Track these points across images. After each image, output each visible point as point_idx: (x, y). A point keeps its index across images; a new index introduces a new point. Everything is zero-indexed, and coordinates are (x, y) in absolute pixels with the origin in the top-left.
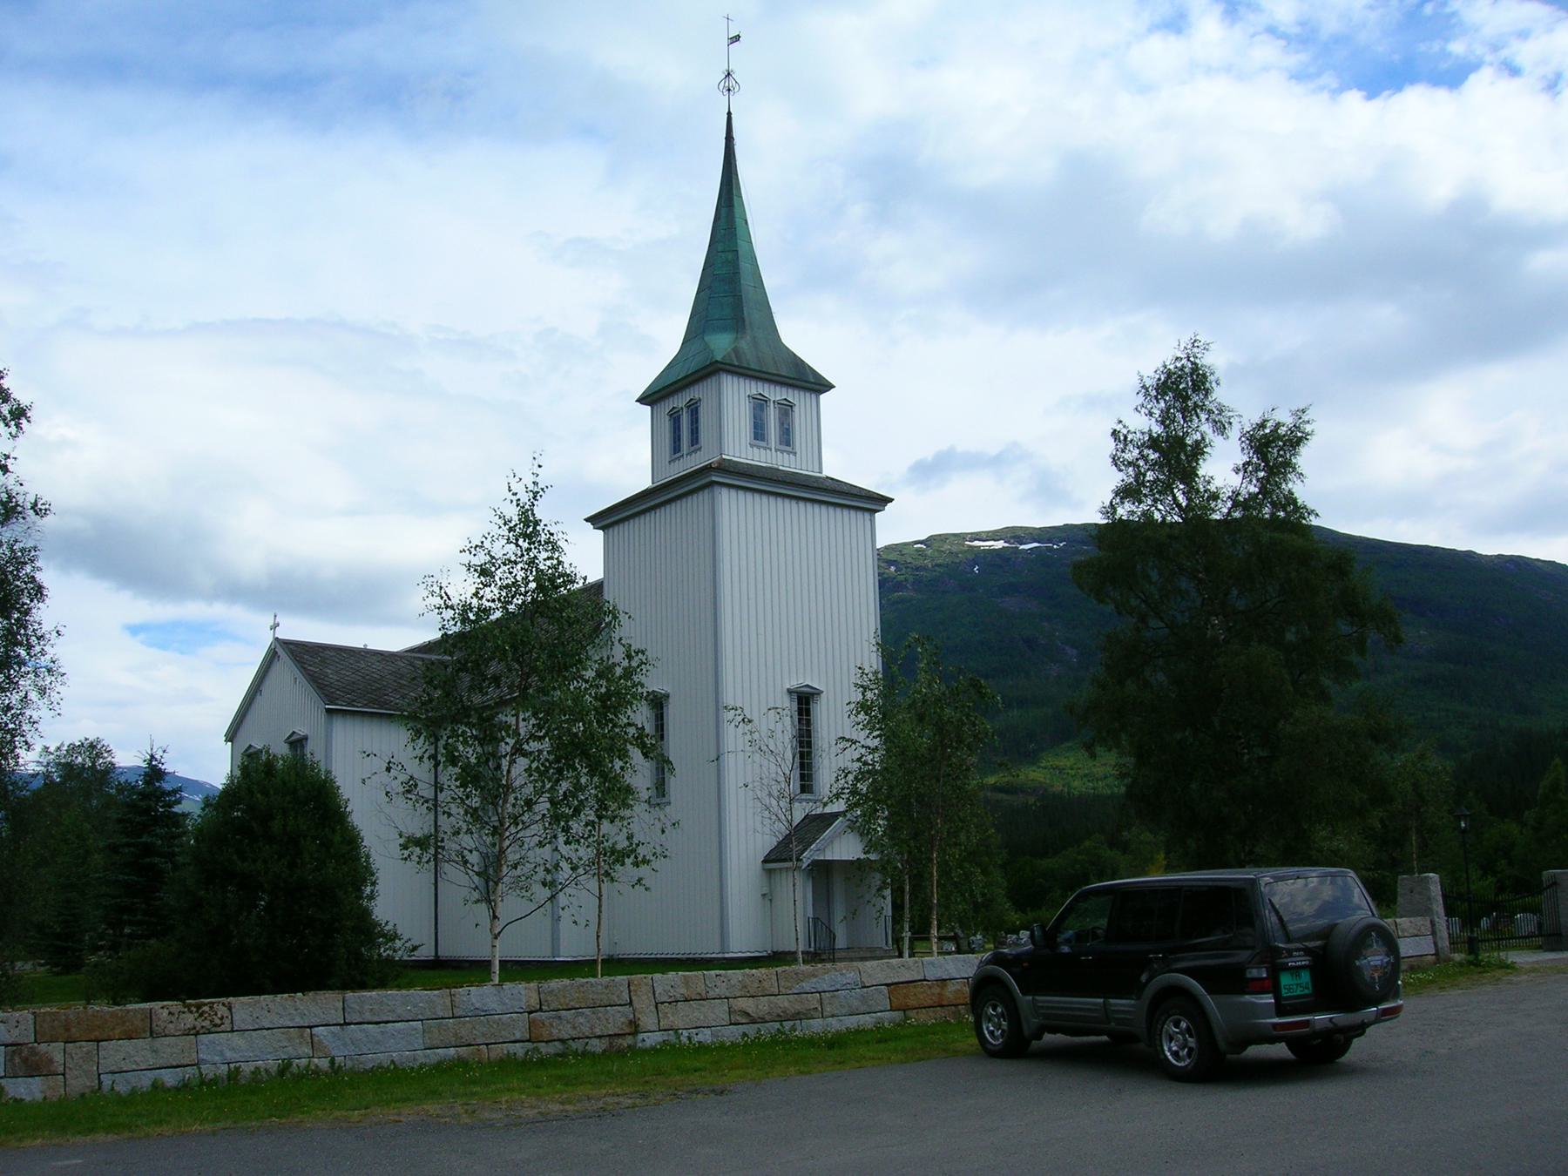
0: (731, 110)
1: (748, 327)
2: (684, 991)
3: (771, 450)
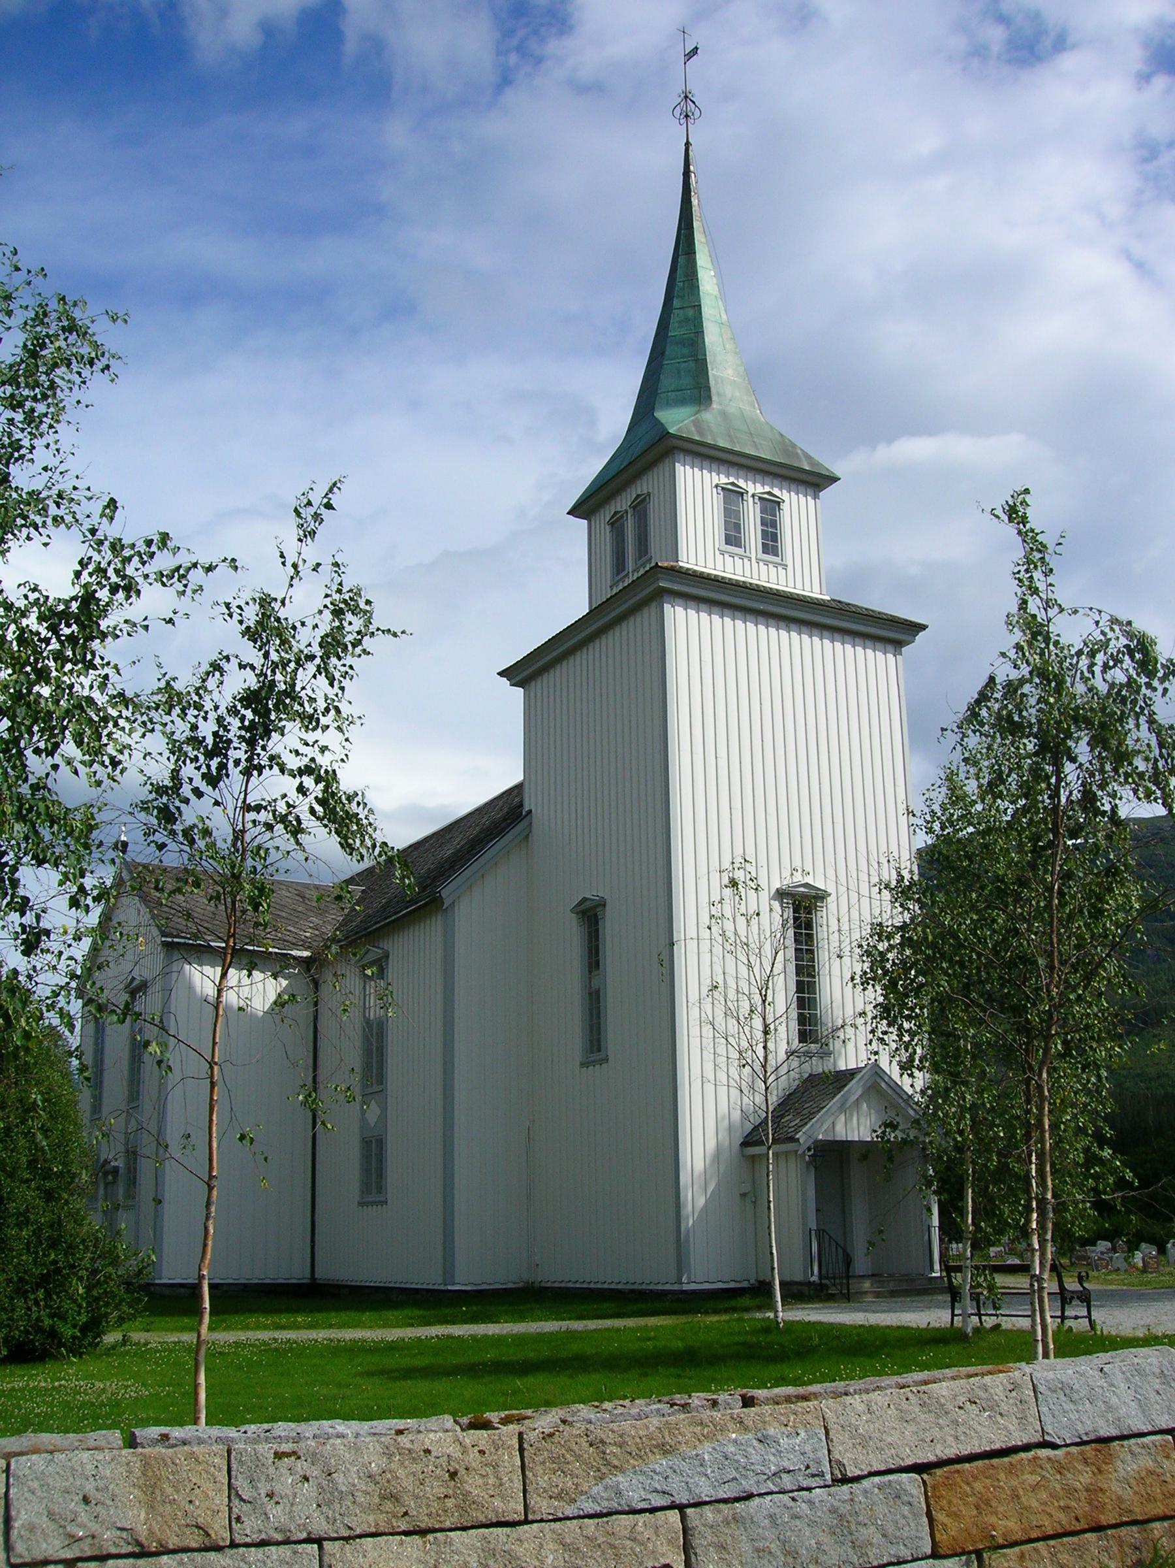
0: (690, 140)
1: (714, 398)
2: (138, 1519)
3: (750, 560)
